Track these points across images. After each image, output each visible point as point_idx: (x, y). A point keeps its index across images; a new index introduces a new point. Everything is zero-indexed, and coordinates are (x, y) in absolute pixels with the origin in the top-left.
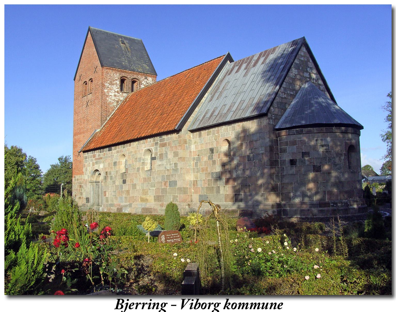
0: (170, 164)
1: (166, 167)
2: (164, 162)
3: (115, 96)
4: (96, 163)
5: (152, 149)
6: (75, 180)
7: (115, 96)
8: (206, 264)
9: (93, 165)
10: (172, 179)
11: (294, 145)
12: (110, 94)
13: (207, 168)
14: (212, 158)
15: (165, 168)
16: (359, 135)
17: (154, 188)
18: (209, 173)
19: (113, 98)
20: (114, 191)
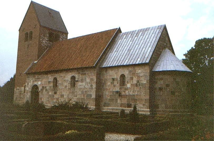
0: (88, 85)
1: (85, 86)
2: (84, 84)
3: (46, 43)
4: (36, 81)
5: (76, 76)
6: (17, 90)
7: (46, 43)
8: (158, 30)
9: (33, 82)
10: (89, 93)
11: (133, 79)
12: (44, 42)
13: (110, 89)
14: (113, 84)
15: (84, 87)
16: (12, 79)
17: (76, 98)
18: (111, 92)
19: (45, 44)
20: (47, 98)
